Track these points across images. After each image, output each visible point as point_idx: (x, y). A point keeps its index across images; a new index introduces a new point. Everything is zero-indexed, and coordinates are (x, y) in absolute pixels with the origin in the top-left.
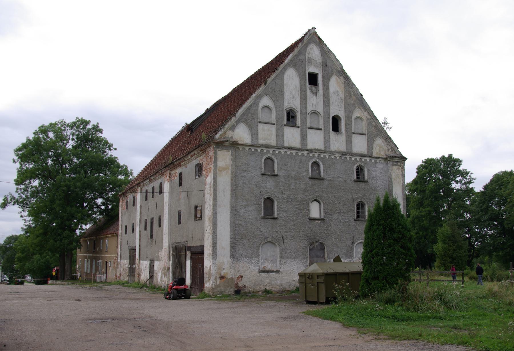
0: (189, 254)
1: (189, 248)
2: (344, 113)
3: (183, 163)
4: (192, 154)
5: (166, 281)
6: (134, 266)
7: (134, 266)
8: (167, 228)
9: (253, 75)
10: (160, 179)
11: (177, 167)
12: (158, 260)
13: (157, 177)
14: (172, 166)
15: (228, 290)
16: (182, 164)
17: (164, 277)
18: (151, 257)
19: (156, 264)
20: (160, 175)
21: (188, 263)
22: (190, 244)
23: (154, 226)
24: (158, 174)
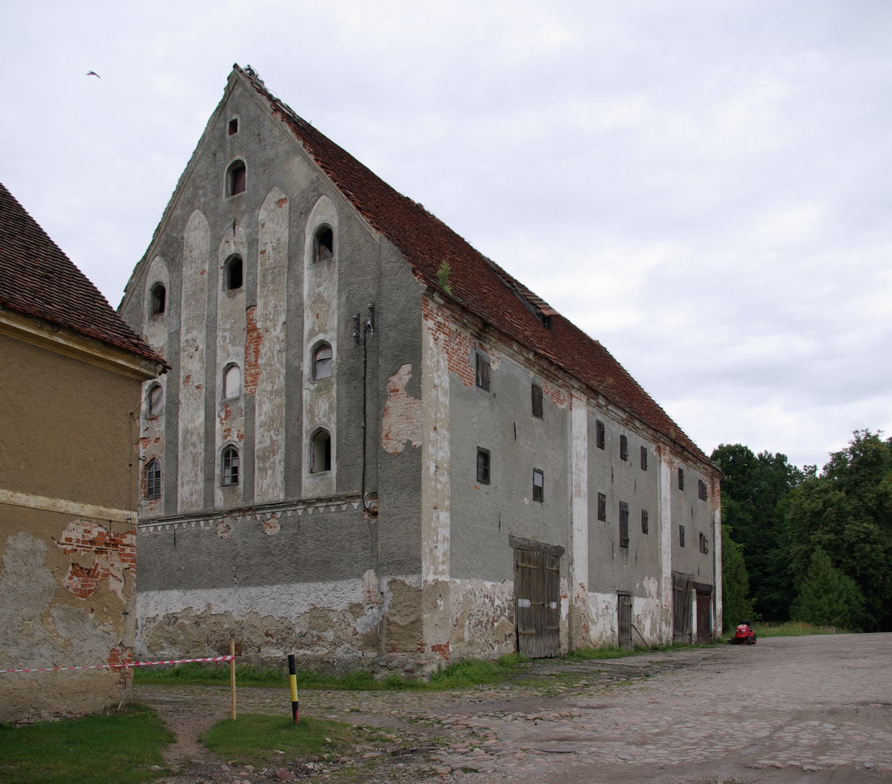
0: (694, 591)
1: (695, 585)
2: (304, 353)
3: (691, 463)
4: (706, 467)
5: (669, 632)
6: (554, 605)
7: (554, 605)
8: (669, 544)
9: (615, 360)
10: (642, 439)
11: (680, 457)
12: (643, 594)
13: (645, 433)
14: (679, 449)
15: (379, 703)
16: (690, 462)
17: (666, 626)
18: (622, 587)
19: (639, 605)
20: (651, 438)
21: (695, 604)
22: (698, 580)
23: (629, 523)
24: (652, 432)
